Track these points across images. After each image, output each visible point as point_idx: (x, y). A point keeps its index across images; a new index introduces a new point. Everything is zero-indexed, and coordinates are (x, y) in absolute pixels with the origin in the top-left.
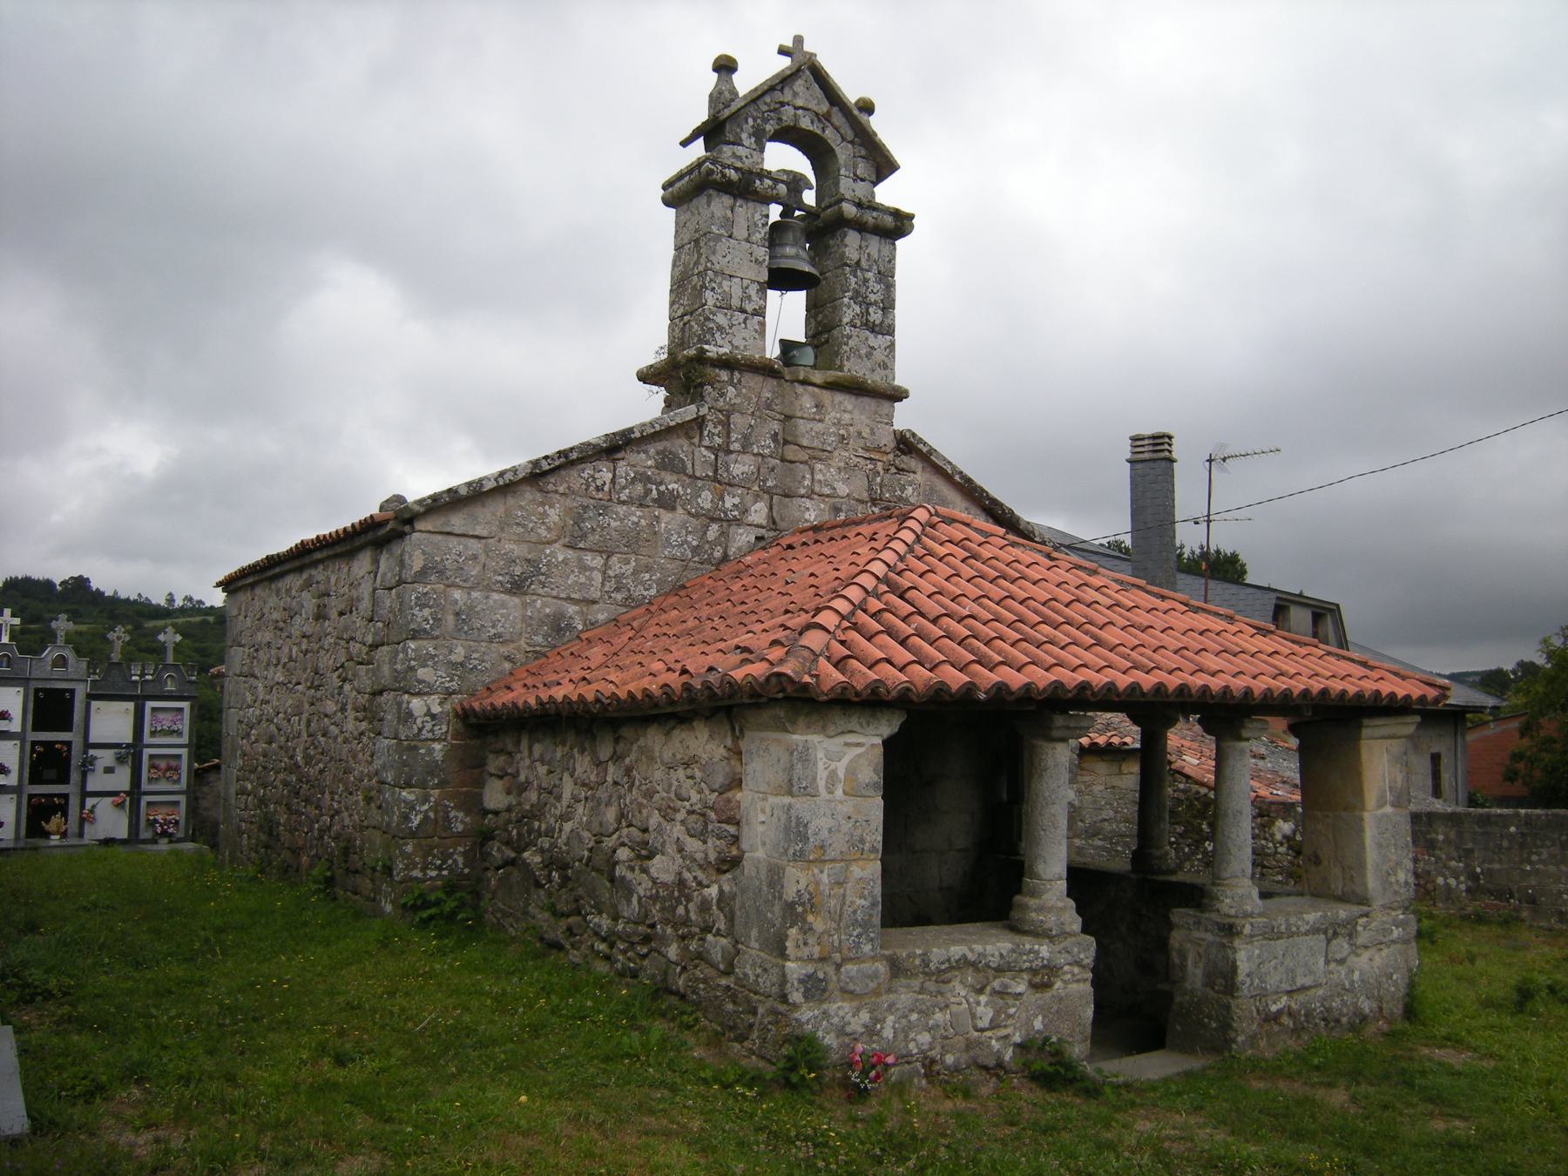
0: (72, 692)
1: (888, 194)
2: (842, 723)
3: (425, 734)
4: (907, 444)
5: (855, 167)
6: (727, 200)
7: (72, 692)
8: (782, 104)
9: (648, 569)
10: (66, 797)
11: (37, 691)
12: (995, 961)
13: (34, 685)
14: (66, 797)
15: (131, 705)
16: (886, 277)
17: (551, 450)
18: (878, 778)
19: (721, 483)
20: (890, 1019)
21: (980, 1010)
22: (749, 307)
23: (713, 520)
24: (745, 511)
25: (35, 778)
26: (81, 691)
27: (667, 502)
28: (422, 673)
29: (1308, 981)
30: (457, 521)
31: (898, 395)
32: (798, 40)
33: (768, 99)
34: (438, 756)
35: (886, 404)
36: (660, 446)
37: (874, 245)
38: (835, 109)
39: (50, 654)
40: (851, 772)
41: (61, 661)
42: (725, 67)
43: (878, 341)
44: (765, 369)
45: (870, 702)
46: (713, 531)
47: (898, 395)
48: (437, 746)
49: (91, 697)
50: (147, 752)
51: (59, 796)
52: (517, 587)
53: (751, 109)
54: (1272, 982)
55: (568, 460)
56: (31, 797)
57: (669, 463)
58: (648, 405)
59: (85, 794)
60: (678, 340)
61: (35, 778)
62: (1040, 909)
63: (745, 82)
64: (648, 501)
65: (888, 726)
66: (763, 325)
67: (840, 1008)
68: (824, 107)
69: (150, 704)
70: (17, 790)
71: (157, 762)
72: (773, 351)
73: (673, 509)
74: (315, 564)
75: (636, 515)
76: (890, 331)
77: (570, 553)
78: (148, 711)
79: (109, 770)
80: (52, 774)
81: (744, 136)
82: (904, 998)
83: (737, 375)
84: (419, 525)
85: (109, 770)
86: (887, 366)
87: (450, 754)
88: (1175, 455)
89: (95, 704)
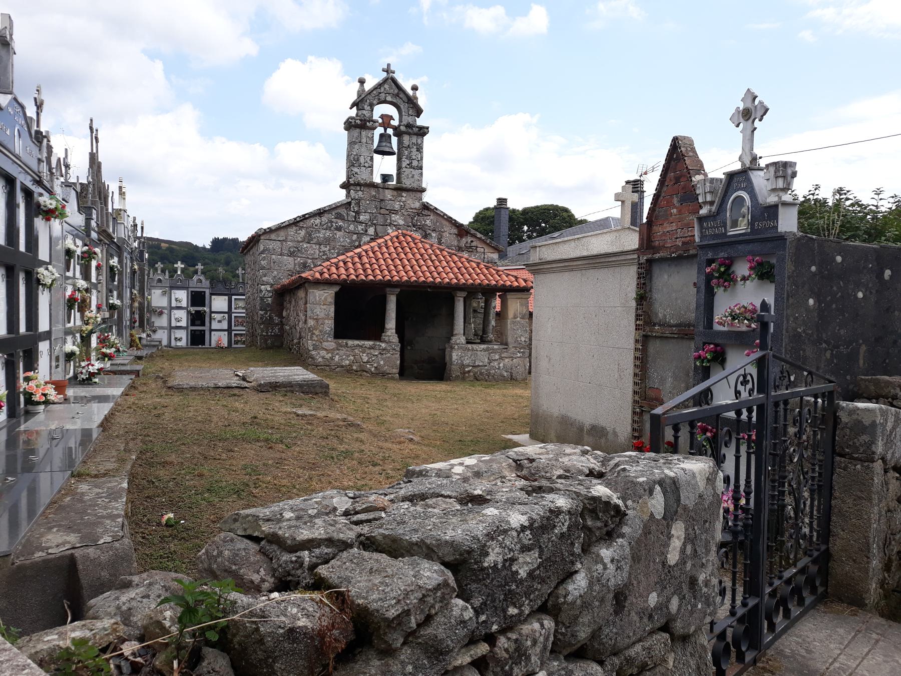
0: (205, 292)
1: (420, 122)
2: (322, 288)
3: (266, 296)
4: (426, 207)
5: (408, 111)
6: (358, 130)
7: (205, 292)
8: (380, 93)
9: (334, 249)
10: (204, 331)
11: (192, 292)
12: (368, 346)
13: (190, 290)
14: (204, 331)
15: (226, 297)
16: (420, 149)
17: (300, 215)
18: (333, 301)
19: (356, 221)
20: (337, 356)
21: (363, 357)
22: (366, 165)
23: (355, 234)
24: (366, 231)
25: (193, 324)
26: (208, 292)
27: (339, 229)
28: (264, 279)
29: (481, 364)
30: (273, 236)
31: (424, 190)
32: (389, 65)
33: (374, 92)
34: (270, 302)
35: (419, 193)
36: (336, 212)
37: (414, 139)
38: (400, 92)
39: (195, 278)
40: (326, 299)
41: (200, 281)
42: (362, 82)
43: (416, 172)
44: (373, 185)
45: (328, 283)
46: (355, 237)
47: (424, 190)
48: (269, 299)
49: (212, 294)
50: (234, 315)
51: (201, 331)
52: (291, 254)
53: (368, 96)
54: (466, 362)
55: (305, 218)
56: (191, 331)
57: (339, 217)
58: (341, 196)
59: (211, 330)
60: (348, 177)
61: (193, 324)
62: (385, 336)
63: (368, 87)
64: (332, 228)
65: (336, 289)
66: (372, 171)
67: (323, 353)
68: (396, 91)
69: (234, 297)
70: (186, 328)
71: (237, 319)
72: (377, 179)
73: (341, 231)
74: (252, 248)
75: (328, 233)
76: (421, 168)
77: (309, 245)
78: (233, 300)
79: (220, 321)
80: (198, 322)
81: (366, 106)
82: (341, 352)
83: (362, 188)
84: (262, 238)
85: (220, 321)
86: (420, 181)
87: (273, 302)
88: (645, 189)
89: (213, 297)
